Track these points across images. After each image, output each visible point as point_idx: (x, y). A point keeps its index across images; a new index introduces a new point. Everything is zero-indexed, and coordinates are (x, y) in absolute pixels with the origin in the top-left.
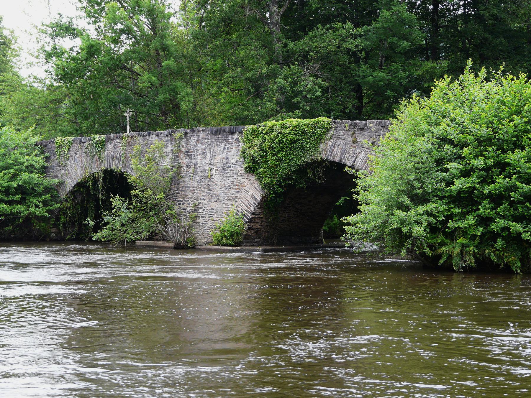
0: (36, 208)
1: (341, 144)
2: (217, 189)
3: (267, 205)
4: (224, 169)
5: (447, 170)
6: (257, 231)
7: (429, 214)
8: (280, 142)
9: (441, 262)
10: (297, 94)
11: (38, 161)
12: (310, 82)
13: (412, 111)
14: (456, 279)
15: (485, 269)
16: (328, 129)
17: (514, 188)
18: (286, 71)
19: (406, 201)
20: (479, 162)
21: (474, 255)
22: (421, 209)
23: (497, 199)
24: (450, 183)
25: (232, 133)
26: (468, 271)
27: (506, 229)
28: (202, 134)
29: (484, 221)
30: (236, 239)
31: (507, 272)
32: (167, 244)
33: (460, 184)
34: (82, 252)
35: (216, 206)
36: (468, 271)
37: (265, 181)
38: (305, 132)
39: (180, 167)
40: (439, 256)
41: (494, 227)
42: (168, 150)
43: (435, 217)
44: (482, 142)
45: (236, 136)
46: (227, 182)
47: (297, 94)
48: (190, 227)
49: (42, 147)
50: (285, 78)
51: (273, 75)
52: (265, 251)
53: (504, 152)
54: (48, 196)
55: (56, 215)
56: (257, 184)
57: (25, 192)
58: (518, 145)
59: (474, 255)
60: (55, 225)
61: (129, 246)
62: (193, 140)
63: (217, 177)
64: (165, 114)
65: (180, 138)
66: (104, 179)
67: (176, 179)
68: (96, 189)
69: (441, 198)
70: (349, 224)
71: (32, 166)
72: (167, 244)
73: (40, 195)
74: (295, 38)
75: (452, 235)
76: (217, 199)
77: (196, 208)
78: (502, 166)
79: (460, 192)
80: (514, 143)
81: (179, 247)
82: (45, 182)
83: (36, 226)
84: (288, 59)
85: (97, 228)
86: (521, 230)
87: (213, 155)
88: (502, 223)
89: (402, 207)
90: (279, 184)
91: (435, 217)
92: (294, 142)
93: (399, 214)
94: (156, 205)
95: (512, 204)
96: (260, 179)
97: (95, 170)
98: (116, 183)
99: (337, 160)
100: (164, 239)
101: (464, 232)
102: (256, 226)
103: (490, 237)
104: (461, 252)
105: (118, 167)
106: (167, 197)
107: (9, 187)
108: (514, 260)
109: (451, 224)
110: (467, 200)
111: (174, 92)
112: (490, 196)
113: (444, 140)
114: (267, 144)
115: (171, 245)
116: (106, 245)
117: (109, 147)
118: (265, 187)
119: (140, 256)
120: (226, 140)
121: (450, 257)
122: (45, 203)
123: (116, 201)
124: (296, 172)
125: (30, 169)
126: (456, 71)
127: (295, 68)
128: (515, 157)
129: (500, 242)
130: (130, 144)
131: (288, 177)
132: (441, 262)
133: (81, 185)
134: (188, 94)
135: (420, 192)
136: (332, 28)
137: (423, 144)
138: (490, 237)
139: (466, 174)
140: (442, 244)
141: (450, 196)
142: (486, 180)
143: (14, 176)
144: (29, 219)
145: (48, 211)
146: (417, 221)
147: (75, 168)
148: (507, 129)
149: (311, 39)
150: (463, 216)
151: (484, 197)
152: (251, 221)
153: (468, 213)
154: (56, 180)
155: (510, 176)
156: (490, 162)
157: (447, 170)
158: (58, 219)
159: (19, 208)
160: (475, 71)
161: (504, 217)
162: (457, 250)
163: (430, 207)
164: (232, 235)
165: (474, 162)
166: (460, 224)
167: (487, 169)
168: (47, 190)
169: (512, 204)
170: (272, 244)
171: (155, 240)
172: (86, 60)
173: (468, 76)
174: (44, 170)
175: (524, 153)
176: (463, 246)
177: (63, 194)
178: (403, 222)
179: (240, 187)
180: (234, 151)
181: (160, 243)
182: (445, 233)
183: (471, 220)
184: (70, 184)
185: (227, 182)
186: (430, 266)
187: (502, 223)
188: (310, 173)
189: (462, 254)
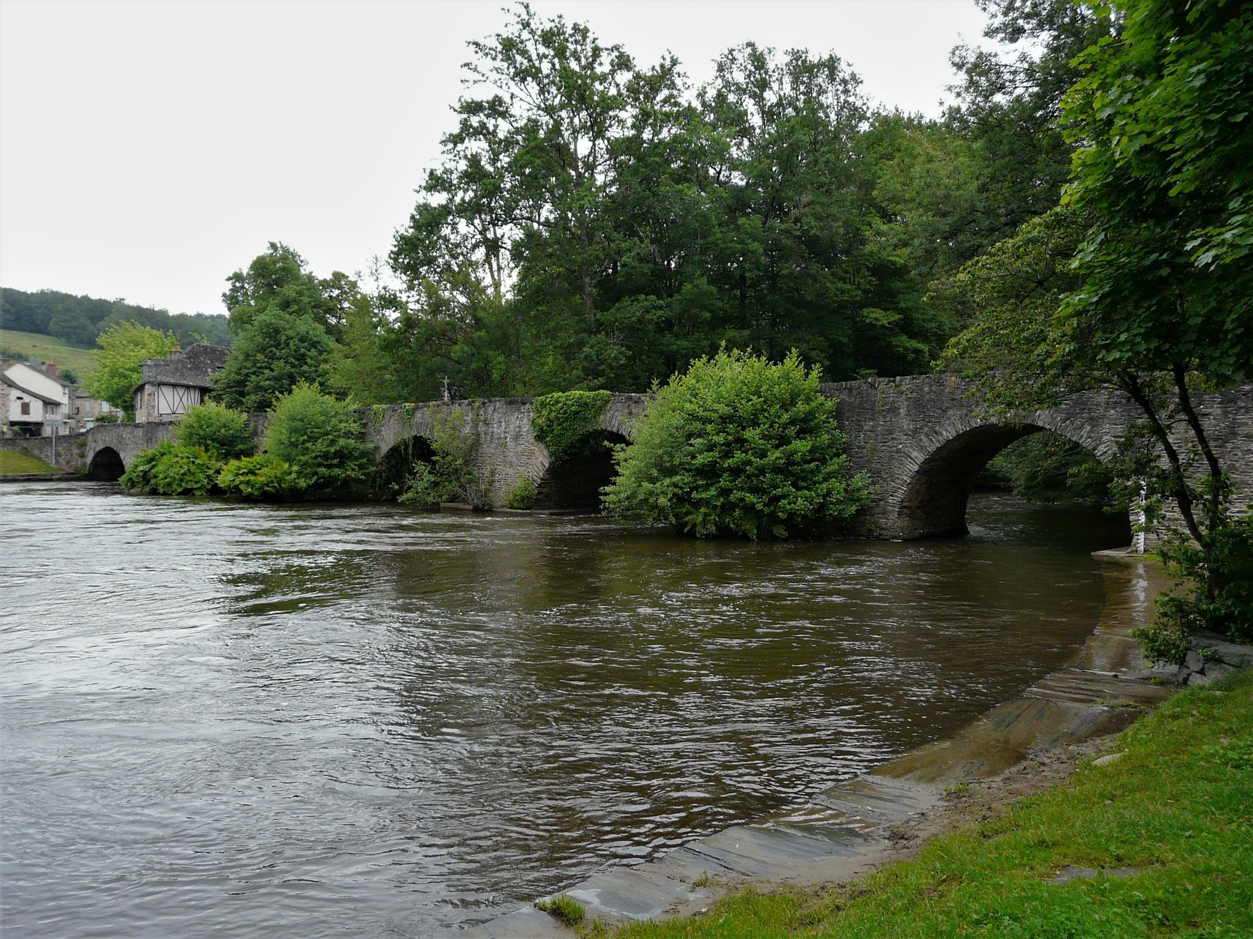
0: (351, 471)
1: (615, 418)
2: (511, 456)
3: (552, 470)
4: (517, 437)
5: (691, 445)
6: (547, 496)
7: (676, 485)
8: (565, 413)
9: (686, 530)
10: (601, 362)
11: (355, 428)
12: (615, 351)
13: (678, 386)
14: (698, 544)
15: (725, 536)
16: (607, 402)
17: (749, 463)
18: (593, 340)
19: (655, 473)
20: (720, 439)
21: (715, 523)
22: (667, 481)
23: (736, 472)
24: (694, 457)
25: (524, 404)
26: (709, 538)
27: (742, 500)
28: (498, 404)
29: (725, 492)
30: (527, 503)
31: (744, 538)
32: (467, 507)
33: (700, 460)
34: (388, 515)
35: (510, 471)
36: (709, 538)
37: (552, 449)
38: (586, 404)
39: (479, 435)
40: (686, 524)
41: (732, 498)
42: (469, 418)
43: (681, 488)
44: (725, 419)
45: (527, 406)
46: (520, 449)
47: (601, 362)
48: (487, 491)
49: (360, 414)
50: (591, 347)
51: (581, 344)
52: (552, 514)
53: (744, 429)
54: (365, 460)
55: (372, 478)
56: (545, 452)
57: (343, 457)
58: (755, 423)
59: (715, 523)
60: (372, 487)
61: (434, 509)
62: (491, 409)
63: (510, 444)
64: (480, 384)
65: (479, 407)
66: (414, 445)
67: (475, 445)
68: (407, 454)
69: (688, 471)
70: (606, 494)
71: (350, 432)
72: (467, 507)
73: (357, 459)
74: (604, 309)
75: (697, 504)
76: (511, 466)
77: (493, 473)
78: (741, 441)
79: (704, 465)
80: (753, 421)
81: (480, 511)
82: (362, 447)
83: (354, 487)
84: (600, 327)
85: (400, 492)
86: (755, 500)
87: (507, 425)
88: (739, 494)
89: (653, 480)
90: (565, 452)
91: (681, 488)
92: (577, 413)
93: (647, 485)
94: (457, 470)
95: (749, 477)
96: (547, 447)
97: (406, 437)
98: (422, 448)
99: (615, 430)
100: (465, 501)
101: (707, 502)
102: (544, 490)
103: (728, 508)
104: (704, 520)
105: (425, 434)
106: (466, 463)
107: (327, 453)
108: (750, 528)
109: (694, 495)
110: (709, 473)
111: (487, 361)
112: (729, 469)
113: (694, 417)
114: (553, 414)
115: (471, 507)
116: (417, 508)
117: (418, 415)
118: (552, 454)
119: (445, 521)
120: (519, 410)
121: (694, 525)
122: (361, 467)
123: (420, 467)
124: (580, 441)
125: (348, 434)
126: (712, 352)
127: (602, 336)
128: (750, 434)
129: (737, 512)
130: (436, 412)
131: (572, 446)
132: (686, 530)
133: (394, 450)
134: (500, 363)
135: (668, 465)
136: (637, 299)
137: (677, 420)
138: (728, 508)
139: (711, 448)
140: (688, 513)
141: (696, 469)
142: (727, 455)
143: (333, 442)
144: (347, 481)
145: (364, 474)
146: (663, 492)
147: (388, 436)
148: (745, 408)
149: (618, 310)
150: (706, 488)
151: (724, 470)
152: (540, 486)
153: (712, 485)
154: (372, 445)
155: (746, 452)
156: (730, 438)
157: (691, 445)
158: (374, 481)
159: (336, 471)
160: (728, 349)
161: (742, 489)
162: (700, 519)
163: (677, 479)
164: (523, 499)
165: (715, 438)
166: (703, 496)
167: (728, 444)
168: (364, 454)
169: (749, 477)
170: (562, 508)
171: (454, 505)
172: (406, 331)
173: (722, 357)
174: (362, 437)
175: (758, 431)
176: (706, 515)
177: (378, 458)
178: (651, 493)
179: (531, 454)
180: (525, 421)
181: (461, 506)
182: (691, 503)
183: (713, 492)
184: (385, 449)
185: (520, 449)
186: (681, 535)
187: (739, 494)
188: (592, 443)
189: (704, 522)
